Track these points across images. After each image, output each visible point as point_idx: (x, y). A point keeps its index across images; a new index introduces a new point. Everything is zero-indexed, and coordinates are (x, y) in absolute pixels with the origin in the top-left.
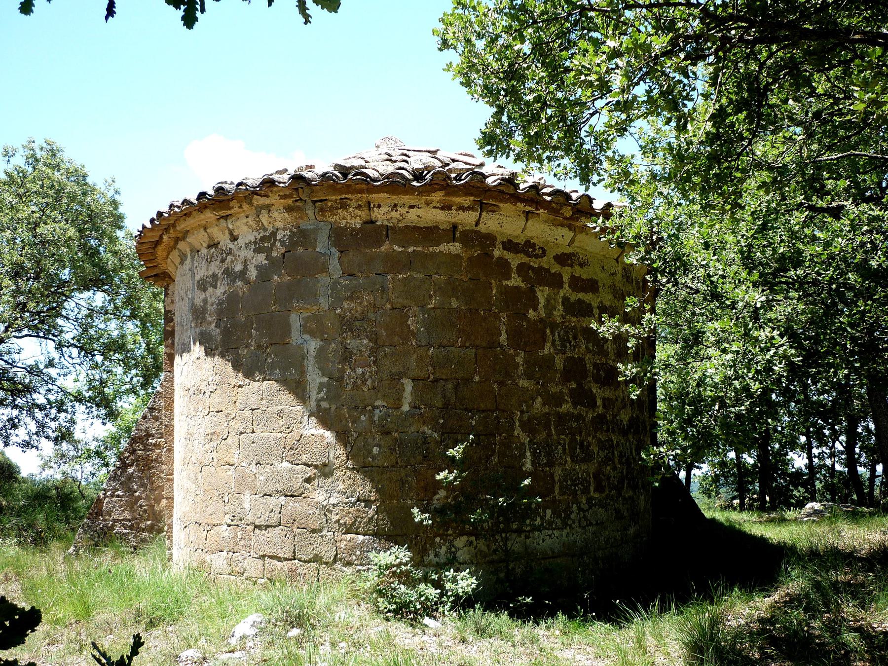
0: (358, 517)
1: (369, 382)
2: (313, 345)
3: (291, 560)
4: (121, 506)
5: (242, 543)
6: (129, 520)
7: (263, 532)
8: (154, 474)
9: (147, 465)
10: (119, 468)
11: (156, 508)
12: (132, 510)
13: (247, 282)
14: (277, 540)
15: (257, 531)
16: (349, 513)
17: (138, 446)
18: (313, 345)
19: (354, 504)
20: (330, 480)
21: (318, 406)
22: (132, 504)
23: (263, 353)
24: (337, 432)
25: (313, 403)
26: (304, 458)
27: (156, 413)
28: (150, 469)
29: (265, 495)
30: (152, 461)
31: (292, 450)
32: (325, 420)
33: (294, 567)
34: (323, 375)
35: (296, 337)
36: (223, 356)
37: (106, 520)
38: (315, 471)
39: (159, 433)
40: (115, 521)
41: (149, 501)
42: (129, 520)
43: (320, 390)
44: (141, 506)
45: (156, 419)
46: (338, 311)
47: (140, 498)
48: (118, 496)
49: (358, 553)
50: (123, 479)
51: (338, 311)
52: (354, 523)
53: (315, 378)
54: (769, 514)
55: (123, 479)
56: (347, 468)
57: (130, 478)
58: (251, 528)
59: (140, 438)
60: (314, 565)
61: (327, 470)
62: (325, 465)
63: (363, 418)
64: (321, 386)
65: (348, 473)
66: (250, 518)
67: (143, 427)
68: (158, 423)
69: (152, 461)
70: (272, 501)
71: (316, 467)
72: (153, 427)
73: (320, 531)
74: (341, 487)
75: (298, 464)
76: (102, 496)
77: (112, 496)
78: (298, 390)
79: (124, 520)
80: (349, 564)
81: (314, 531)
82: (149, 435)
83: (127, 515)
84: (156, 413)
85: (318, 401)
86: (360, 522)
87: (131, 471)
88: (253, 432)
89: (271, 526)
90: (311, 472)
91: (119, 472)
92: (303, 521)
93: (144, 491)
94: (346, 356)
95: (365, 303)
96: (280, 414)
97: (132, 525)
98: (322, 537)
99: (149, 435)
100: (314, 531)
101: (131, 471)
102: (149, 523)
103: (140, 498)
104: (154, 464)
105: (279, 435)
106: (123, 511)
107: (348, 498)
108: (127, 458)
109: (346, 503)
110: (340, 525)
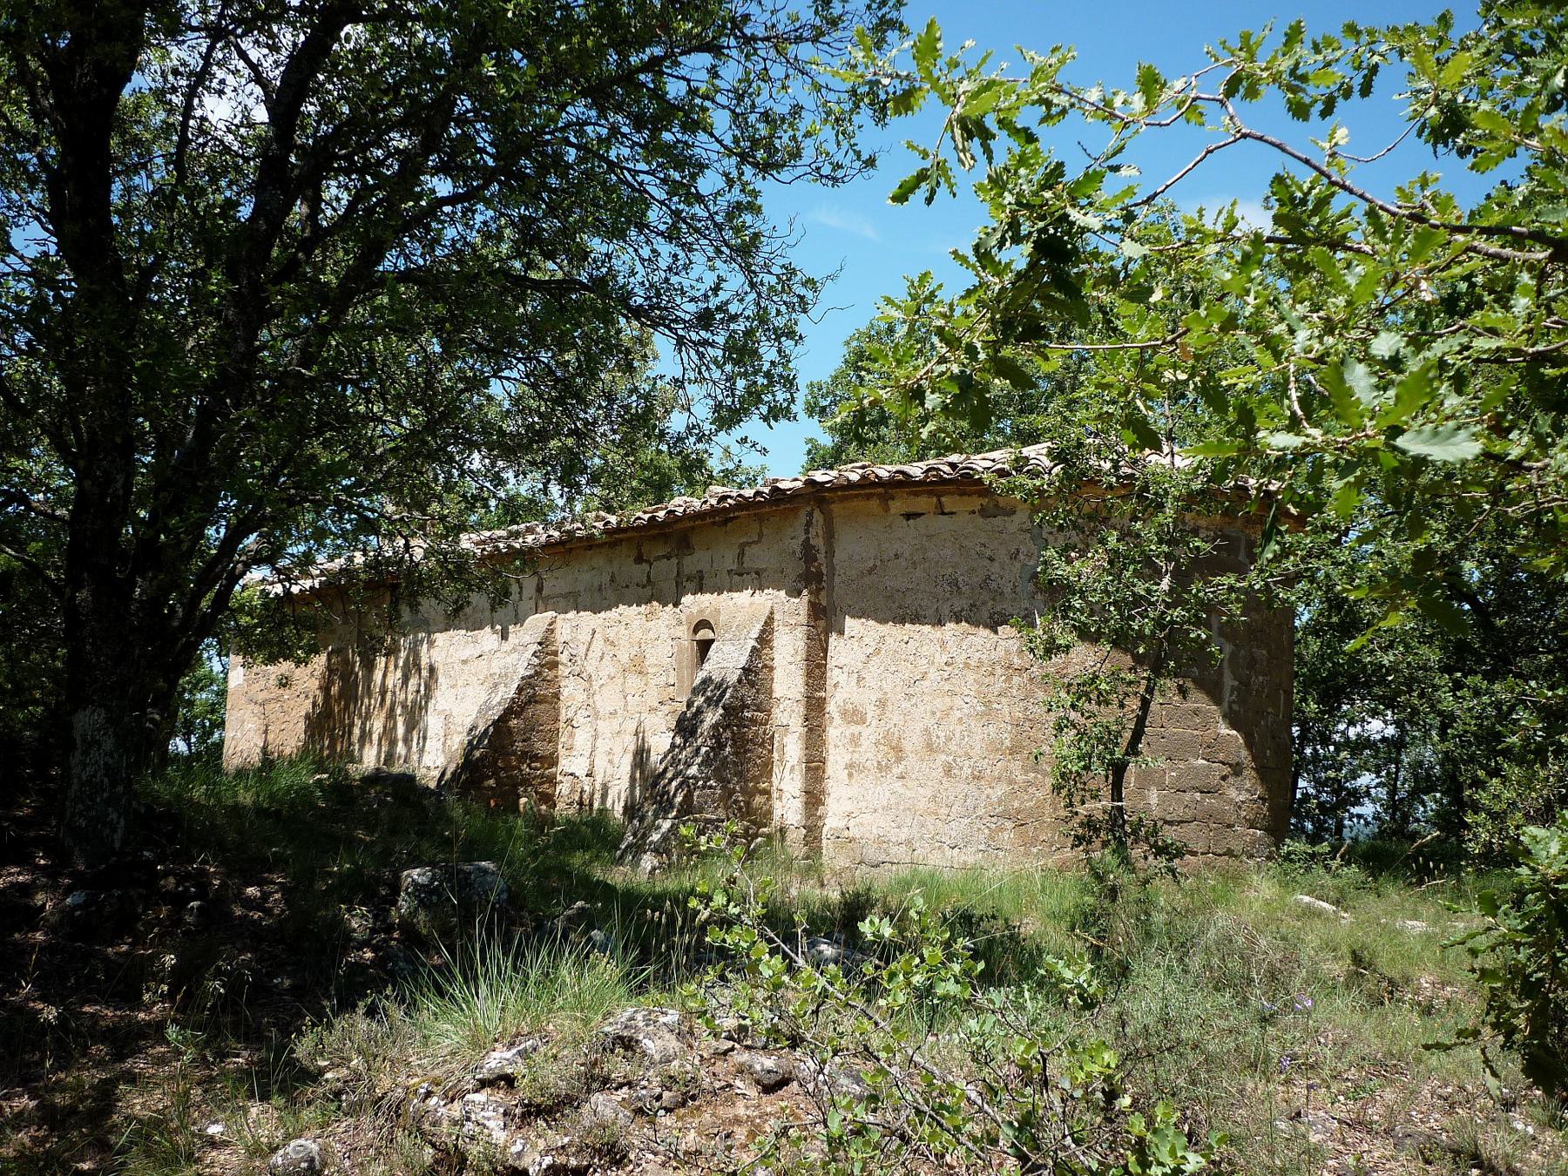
9: (742, 745)
25: (1226, 705)
26: (1221, 756)
28: (746, 752)
31: (1211, 749)
32: (1233, 725)
45: (752, 684)
48: (711, 787)
53: (1229, 681)
54: (1287, 884)
64: (1233, 688)
70: (1187, 796)
72: (748, 694)
74: (1248, 785)
77: (704, 787)
78: (1215, 695)
80: (1251, 856)
81: (1229, 826)
85: (1230, 703)
90: (1226, 770)
94: (1252, 663)
96: (1196, 712)
99: (745, 707)
100: (1229, 826)
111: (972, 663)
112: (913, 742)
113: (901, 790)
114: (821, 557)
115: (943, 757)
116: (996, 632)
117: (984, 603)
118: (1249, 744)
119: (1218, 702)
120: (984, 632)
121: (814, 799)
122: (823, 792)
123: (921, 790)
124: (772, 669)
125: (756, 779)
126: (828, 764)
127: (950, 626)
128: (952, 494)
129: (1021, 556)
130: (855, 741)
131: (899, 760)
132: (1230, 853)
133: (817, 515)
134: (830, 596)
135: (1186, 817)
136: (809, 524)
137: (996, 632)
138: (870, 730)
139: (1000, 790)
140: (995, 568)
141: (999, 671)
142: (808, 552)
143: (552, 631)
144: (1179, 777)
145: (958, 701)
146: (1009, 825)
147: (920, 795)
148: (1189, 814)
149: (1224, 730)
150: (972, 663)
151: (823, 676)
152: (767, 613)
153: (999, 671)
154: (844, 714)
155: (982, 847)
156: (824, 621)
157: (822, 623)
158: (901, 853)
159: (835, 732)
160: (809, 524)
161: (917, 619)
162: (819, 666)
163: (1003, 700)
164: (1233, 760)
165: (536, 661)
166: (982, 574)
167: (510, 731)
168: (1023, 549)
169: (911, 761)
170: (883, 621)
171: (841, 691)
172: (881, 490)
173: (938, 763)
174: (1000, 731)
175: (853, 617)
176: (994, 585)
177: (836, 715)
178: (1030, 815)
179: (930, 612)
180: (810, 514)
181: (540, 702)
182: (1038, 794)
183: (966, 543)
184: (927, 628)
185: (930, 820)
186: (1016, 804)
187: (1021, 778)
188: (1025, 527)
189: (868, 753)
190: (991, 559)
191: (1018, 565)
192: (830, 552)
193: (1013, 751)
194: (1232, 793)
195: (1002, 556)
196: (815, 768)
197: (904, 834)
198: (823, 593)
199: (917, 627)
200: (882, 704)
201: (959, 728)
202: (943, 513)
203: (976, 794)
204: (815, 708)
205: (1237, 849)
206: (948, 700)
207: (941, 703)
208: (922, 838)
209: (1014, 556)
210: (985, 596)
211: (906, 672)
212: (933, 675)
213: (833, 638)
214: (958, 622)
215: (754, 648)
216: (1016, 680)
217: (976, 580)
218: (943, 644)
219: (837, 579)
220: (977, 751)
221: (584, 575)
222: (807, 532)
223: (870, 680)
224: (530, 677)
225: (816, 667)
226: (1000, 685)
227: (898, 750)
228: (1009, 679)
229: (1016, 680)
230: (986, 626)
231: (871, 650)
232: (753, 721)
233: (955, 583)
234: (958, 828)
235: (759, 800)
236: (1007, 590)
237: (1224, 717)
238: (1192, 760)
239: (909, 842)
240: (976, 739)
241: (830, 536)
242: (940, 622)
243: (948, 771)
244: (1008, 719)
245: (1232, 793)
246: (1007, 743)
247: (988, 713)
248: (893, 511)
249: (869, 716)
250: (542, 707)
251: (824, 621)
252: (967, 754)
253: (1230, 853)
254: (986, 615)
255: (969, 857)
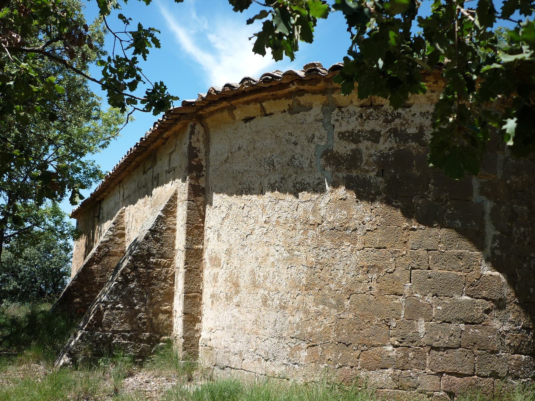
0: (522, 341)
1: (528, 239)
2: (489, 205)
3: (471, 376)
4: (121, 319)
5: (414, 361)
6: (128, 332)
7: (441, 353)
8: (153, 290)
10: (120, 283)
11: (154, 321)
12: (131, 323)
13: (422, 144)
14: (457, 359)
15: (433, 352)
16: (517, 338)
17: (138, 264)
18: (489, 205)
19: (520, 331)
20: (503, 312)
21: (493, 253)
22: (132, 316)
23: (442, 205)
24: (508, 275)
25: (488, 250)
26: (484, 293)
27: (157, 236)
28: (150, 285)
29: (444, 322)
30: (152, 278)
31: (474, 288)
32: (496, 267)
33: (474, 382)
34: (497, 229)
35: (476, 197)
36: (388, 202)
37: (105, 331)
38: (492, 304)
39: (159, 254)
40: (114, 332)
41: (147, 314)
42: (128, 332)
43: (494, 242)
44: (140, 319)
45: (157, 240)
46: (508, 182)
47: (139, 311)
48: (119, 308)
49: (522, 369)
50: (124, 293)
51: (508, 182)
52: (519, 346)
53: (490, 231)
55: (124, 293)
56: (515, 303)
57: (131, 292)
58: (427, 349)
59: (141, 256)
60: (492, 379)
61: (501, 303)
62: (501, 300)
63: (525, 265)
64: (495, 238)
65: (516, 307)
66: (424, 340)
67: (146, 247)
68: (159, 244)
69: (152, 278)
70: (453, 327)
71: (494, 301)
72: (154, 248)
73: (497, 352)
74: (511, 317)
75: (477, 298)
76: (102, 309)
77: (112, 308)
78: (478, 241)
79: (124, 331)
80: (516, 378)
81: (493, 352)
82: (150, 255)
83: (126, 326)
84: (157, 236)
85: (493, 250)
86: (523, 345)
87: (132, 286)
88: (429, 269)
89: (451, 348)
90: (489, 305)
91: (120, 287)
92: (483, 344)
93: (143, 306)
95: (524, 180)
96: (460, 257)
97: (131, 336)
98: (498, 356)
99: (150, 255)
100: (493, 352)
101: (132, 286)
102: (147, 334)
103: (139, 311)
104: (154, 281)
105: (459, 273)
106: (123, 323)
107: (516, 326)
108: (129, 274)
109: (515, 330)
110: (511, 347)
111: (281, 221)
112: (244, 281)
113: (237, 315)
114: (201, 155)
115: (262, 291)
116: (297, 197)
117: (290, 176)
118: (512, 281)
119: (480, 247)
120: (289, 197)
121: (192, 318)
122: (200, 313)
123: (249, 316)
124: (174, 230)
125: (160, 303)
126: (203, 294)
127: (268, 194)
128: (268, 99)
129: (316, 140)
130: (215, 278)
131: (237, 292)
132: (495, 375)
133: (199, 128)
134: (207, 180)
135: (451, 344)
136: (192, 133)
137: (297, 197)
138: (223, 270)
139: (298, 318)
140: (298, 150)
141: (299, 226)
142: (192, 153)
143: (122, 217)
144: (444, 311)
145: (272, 250)
146: (304, 345)
147: (247, 318)
148: (455, 341)
149: (487, 271)
150: (281, 221)
151: (201, 234)
152: (172, 193)
153: (299, 226)
154: (211, 259)
155: (285, 361)
156: (200, 196)
157: (201, 199)
158: (235, 361)
159: (207, 273)
160: (192, 133)
161: (249, 191)
162: (197, 228)
163: (302, 248)
164: (496, 296)
165: (111, 233)
166: (289, 155)
167: (92, 272)
168: (317, 134)
169: (244, 293)
170: (230, 194)
171: (212, 245)
172: (224, 104)
173: (259, 296)
174: (299, 272)
175: (216, 193)
176: (297, 162)
177: (207, 260)
178: (319, 339)
179: (257, 185)
180: (193, 127)
181: (113, 255)
182: (325, 322)
183: (279, 134)
184: (254, 197)
185: (254, 337)
186: (309, 329)
187: (313, 309)
188: (319, 118)
189: (222, 288)
190: (296, 144)
191: (313, 146)
192: (207, 153)
193: (308, 287)
194: (496, 324)
195: (303, 140)
196: (193, 297)
197: (238, 347)
198: (202, 179)
199: (249, 197)
200: (228, 252)
201: (272, 270)
202: (266, 115)
203: (282, 320)
204: (194, 255)
205: (502, 372)
206: (266, 248)
207: (261, 251)
208: (248, 351)
209: (311, 140)
210: (291, 170)
211: (244, 229)
212: (258, 231)
213: (208, 206)
214: (273, 191)
215: (160, 216)
216: (311, 232)
217: (286, 159)
218: (264, 207)
219: (211, 169)
220: (282, 288)
221: (129, 187)
222: (190, 138)
223: (224, 237)
224: (107, 242)
225: (196, 229)
226: (299, 237)
227: (236, 285)
228: (306, 231)
229: (311, 232)
230: (291, 193)
231: (224, 216)
232: (157, 265)
233: (272, 164)
234: (269, 345)
235: (162, 317)
236: (306, 165)
237: (487, 260)
238: (456, 297)
239: (240, 353)
240: (284, 278)
241: (207, 141)
242: (262, 193)
243: (265, 302)
244: (304, 263)
245: (496, 324)
246: (304, 281)
247: (291, 260)
248: (237, 118)
249: (222, 261)
250: (114, 258)
251: (200, 196)
252: (276, 290)
253: (495, 375)
254: (291, 184)
255: (276, 368)
